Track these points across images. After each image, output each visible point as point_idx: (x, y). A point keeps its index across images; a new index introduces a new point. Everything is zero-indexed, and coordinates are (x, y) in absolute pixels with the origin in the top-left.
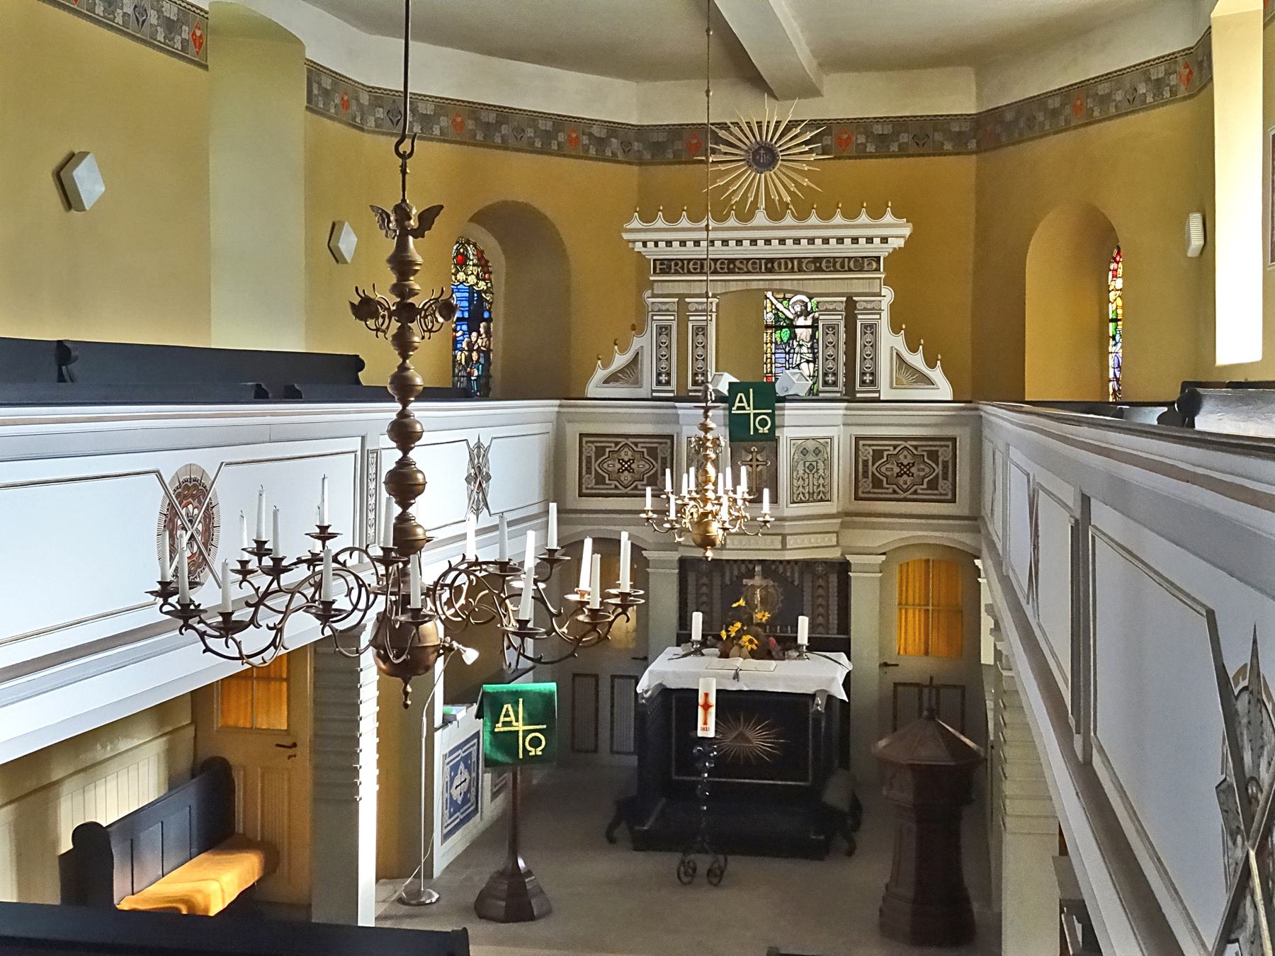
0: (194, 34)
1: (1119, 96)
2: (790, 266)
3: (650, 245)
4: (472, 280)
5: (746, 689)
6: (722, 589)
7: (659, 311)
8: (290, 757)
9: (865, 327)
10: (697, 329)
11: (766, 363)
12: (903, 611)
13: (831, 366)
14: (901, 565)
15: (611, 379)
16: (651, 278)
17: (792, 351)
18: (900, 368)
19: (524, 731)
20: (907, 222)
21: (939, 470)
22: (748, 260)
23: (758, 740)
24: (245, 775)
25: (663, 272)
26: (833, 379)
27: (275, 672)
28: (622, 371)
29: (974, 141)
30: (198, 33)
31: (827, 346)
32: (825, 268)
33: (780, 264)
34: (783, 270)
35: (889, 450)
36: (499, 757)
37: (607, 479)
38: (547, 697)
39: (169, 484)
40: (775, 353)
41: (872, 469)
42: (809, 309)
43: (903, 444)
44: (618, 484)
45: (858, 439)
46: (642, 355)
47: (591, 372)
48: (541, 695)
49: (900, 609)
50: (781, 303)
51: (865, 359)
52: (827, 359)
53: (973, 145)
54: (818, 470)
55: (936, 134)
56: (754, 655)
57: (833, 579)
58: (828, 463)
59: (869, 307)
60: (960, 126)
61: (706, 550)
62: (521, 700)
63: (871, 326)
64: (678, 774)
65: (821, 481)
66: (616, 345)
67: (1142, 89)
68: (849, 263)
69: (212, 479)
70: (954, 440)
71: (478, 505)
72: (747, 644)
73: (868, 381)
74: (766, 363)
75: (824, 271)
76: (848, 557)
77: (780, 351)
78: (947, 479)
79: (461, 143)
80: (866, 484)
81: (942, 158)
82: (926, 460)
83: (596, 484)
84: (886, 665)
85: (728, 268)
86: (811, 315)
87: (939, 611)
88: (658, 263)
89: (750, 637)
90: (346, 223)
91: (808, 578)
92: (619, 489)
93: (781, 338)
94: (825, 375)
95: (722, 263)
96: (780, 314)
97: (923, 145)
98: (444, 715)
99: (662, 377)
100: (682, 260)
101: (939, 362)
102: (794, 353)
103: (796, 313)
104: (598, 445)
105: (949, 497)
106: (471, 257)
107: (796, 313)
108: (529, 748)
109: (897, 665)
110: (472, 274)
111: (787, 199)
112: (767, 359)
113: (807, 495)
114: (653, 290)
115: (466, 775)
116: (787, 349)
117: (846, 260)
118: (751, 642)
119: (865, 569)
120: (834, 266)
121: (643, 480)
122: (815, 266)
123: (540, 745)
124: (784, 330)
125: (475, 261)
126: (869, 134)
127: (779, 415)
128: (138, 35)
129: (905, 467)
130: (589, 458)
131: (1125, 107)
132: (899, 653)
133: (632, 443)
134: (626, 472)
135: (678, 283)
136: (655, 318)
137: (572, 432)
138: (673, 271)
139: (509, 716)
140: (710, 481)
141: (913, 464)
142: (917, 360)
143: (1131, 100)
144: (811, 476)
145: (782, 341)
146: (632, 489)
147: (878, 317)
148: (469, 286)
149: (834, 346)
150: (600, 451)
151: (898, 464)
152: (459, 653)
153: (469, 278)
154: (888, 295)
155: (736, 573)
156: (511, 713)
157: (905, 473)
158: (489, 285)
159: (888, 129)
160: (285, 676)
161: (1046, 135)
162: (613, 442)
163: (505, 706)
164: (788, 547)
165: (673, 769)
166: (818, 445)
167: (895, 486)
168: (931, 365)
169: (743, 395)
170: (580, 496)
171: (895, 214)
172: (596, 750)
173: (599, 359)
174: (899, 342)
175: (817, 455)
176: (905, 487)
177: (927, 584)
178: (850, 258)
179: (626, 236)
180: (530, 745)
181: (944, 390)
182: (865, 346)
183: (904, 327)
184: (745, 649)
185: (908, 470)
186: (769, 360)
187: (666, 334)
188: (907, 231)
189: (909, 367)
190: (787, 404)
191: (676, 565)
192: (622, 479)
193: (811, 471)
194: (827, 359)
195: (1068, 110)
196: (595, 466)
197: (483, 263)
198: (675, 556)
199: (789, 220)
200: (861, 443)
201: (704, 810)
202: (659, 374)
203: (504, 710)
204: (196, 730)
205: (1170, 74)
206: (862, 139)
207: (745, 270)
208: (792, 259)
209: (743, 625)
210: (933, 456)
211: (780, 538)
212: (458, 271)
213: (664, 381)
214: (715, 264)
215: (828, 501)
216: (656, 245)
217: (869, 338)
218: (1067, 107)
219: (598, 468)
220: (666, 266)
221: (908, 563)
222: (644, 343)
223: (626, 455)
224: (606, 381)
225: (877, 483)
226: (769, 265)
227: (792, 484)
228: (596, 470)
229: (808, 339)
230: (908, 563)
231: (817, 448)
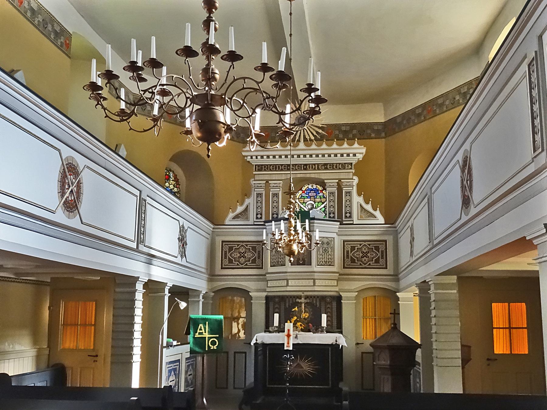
0: (66, 42)
1: (447, 102)
2: (314, 167)
3: (254, 157)
4: (172, 187)
5: (301, 343)
6: (285, 310)
7: (258, 187)
8: (94, 361)
9: (346, 193)
10: (274, 194)
12: (365, 319)
13: (332, 210)
14: (363, 299)
15: (236, 217)
16: (254, 173)
18: (361, 211)
19: (208, 337)
20: (364, 147)
21: (380, 254)
22: (296, 165)
23: (306, 367)
24: (72, 371)
25: (259, 170)
26: (333, 215)
27: (92, 304)
28: (240, 214)
29: (384, 133)
30: (68, 42)
31: (330, 201)
32: (329, 168)
33: (309, 167)
34: (311, 169)
35: (358, 246)
36: (197, 349)
37: (234, 261)
38: (219, 322)
39: (64, 159)
41: (350, 255)
43: (364, 243)
44: (239, 263)
45: (344, 241)
46: (250, 207)
47: (226, 216)
48: (216, 320)
49: (363, 318)
50: (303, 204)
51: (347, 207)
52: (330, 207)
53: (383, 135)
54: (328, 251)
55: (368, 130)
56: (302, 330)
57: (334, 304)
58: (333, 249)
59: (348, 184)
60: (378, 127)
61: (290, 257)
62: (207, 322)
63: (349, 192)
64: (269, 384)
65: (330, 257)
66: (238, 202)
67: (457, 98)
68: (339, 166)
69: (81, 170)
70: (386, 241)
71: (182, 254)
72: (299, 326)
73: (348, 216)
75: (328, 169)
76: (341, 293)
78: (383, 259)
79: (170, 123)
80: (348, 261)
81: (371, 140)
82: (374, 250)
83: (229, 263)
84: (357, 344)
85: (287, 168)
87: (380, 319)
88: (257, 166)
89: (300, 323)
90: (123, 145)
91: (323, 304)
92: (239, 265)
94: (330, 214)
95: (284, 166)
96: (302, 209)
97: (363, 134)
98: (167, 342)
99: (258, 215)
100: (267, 165)
101: (378, 208)
103: (309, 209)
104: (230, 246)
105: (384, 266)
106: (172, 177)
107: (309, 209)
108: (210, 346)
109: (363, 344)
110: (172, 184)
111: (313, 138)
113: (324, 262)
114: (254, 178)
115: (174, 378)
117: (338, 164)
118: (301, 325)
119: (348, 299)
120: (333, 167)
121: (250, 261)
122: (325, 167)
123: (216, 344)
125: (173, 179)
126: (340, 131)
127: (312, 226)
128: (44, 32)
129: (365, 253)
130: (226, 252)
131: (451, 106)
132: (363, 339)
133: (245, 245)
134: (242, 258)
135: (265, 175)
136: (255, 190)
137: (219, 240)
138: (263, 170)
139: (202, 330)
140: (292, 226)
141: (368, 252)
142: (369, 207)
143: (453, 103)
144: (325, 254)
146: (245, 266)
147: (352, 188)
148: (170, 189)
149: (333, 201)
150: (231, 249)
151: (362, 252)
152: (178, 304)
153: (171, 186)
154: (356, 180)
155: (291, 302)
156: (203, 328)
157: (365, 256)
158: (179, 190)
159: (348, 128)
160: (93, 323)
161: (416, 125)
162: (236, 244)
163: (200, 325)
164: (316, 285)
165: (267, 383)
166: (328, 241)
167: (360, 262)
168: (375, 210)
170: (221, 269)
171: (359, 144)
172: (227, 388)
173: (231, 209)
174: (361, 200)
175: (328, 245)
176: (365, 262)
177: (375, 309)
178: (339, 164)
179: (244, 154)
180: (211, 345)
181: (381, 220)
182: (347, 201)
183: (363, 193)
184: (298, 328)
185: (366, 255)
187: (260, 197)
188: (364, 151)
189: (365, 210)
190: (315, 221)
191: (264, 299)
192: (241, 261)
193: (325, 252)
194: (330, 207)
195: (425, 112)
196: (228, 255)
197: (176, 180)
198: (265, 294)
199: (314, 146)
200: (346, 243)
202: (257, 214)
203: (199, 327)
204: (49, 351)
205: (470, 89)
206: (337, 132)
207: (295, 169)
208: (315, 164)
209: (297, 318)
210: (377, 248)
211: (312, 280)
212: (166, 182)
213: (259, 217)
214: (282, 167)
215: (333, 266)
216: (257, 158)
217: (348, 197)
218: (425, 111)
219: (230, 256)
220: (260, 168)
221: (366, 298)
222: (250, 201)
223: (242, 250)
224: (234, 218)
225: (353, 261)
226: (305, 167)
227: (317, 257)
228: (229, 257)
230: (366, 298)
231: (328, 242)
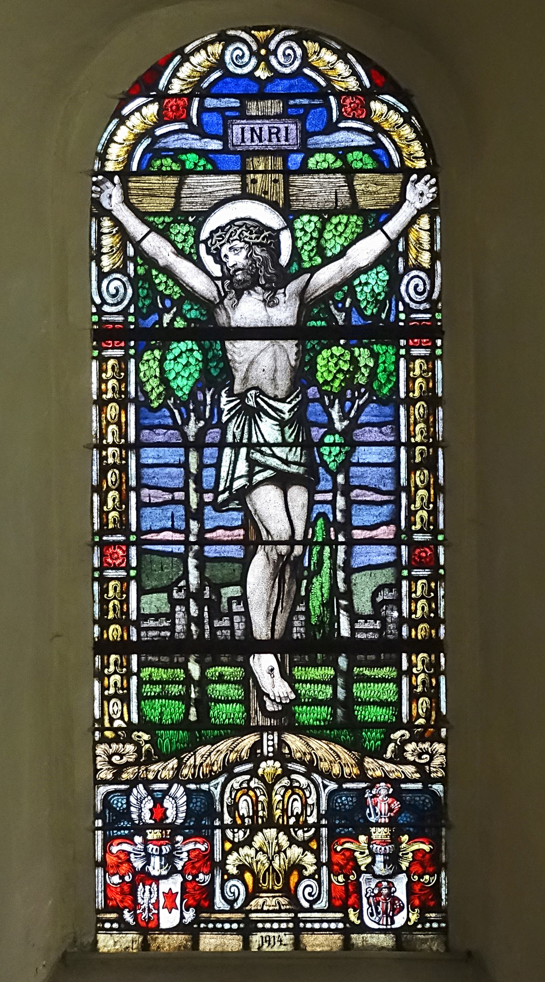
11: (97, 489)
17: (213, 435)
40: (139, 445)
42: (284, 259)
50: (164, 233)
74: (123, 120)
77: (160, 436)
86: (294, 286)
93: (164, 380)
102: (222, 445)
112: (104, 471)
116: (192, 429)
124: (177, 347)
145: (169, 392)
169: (136, 733)
186: (111, 477)
201: (157, 328)
229: (283, 383)
